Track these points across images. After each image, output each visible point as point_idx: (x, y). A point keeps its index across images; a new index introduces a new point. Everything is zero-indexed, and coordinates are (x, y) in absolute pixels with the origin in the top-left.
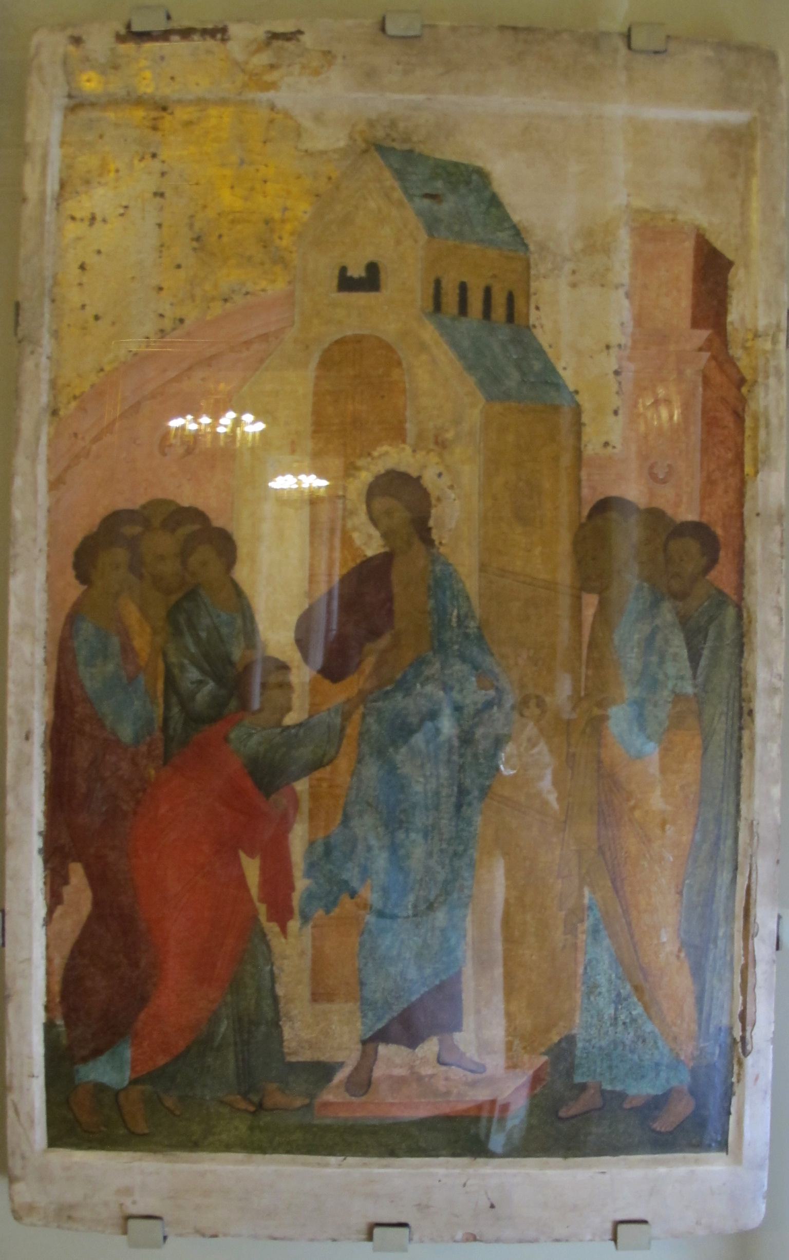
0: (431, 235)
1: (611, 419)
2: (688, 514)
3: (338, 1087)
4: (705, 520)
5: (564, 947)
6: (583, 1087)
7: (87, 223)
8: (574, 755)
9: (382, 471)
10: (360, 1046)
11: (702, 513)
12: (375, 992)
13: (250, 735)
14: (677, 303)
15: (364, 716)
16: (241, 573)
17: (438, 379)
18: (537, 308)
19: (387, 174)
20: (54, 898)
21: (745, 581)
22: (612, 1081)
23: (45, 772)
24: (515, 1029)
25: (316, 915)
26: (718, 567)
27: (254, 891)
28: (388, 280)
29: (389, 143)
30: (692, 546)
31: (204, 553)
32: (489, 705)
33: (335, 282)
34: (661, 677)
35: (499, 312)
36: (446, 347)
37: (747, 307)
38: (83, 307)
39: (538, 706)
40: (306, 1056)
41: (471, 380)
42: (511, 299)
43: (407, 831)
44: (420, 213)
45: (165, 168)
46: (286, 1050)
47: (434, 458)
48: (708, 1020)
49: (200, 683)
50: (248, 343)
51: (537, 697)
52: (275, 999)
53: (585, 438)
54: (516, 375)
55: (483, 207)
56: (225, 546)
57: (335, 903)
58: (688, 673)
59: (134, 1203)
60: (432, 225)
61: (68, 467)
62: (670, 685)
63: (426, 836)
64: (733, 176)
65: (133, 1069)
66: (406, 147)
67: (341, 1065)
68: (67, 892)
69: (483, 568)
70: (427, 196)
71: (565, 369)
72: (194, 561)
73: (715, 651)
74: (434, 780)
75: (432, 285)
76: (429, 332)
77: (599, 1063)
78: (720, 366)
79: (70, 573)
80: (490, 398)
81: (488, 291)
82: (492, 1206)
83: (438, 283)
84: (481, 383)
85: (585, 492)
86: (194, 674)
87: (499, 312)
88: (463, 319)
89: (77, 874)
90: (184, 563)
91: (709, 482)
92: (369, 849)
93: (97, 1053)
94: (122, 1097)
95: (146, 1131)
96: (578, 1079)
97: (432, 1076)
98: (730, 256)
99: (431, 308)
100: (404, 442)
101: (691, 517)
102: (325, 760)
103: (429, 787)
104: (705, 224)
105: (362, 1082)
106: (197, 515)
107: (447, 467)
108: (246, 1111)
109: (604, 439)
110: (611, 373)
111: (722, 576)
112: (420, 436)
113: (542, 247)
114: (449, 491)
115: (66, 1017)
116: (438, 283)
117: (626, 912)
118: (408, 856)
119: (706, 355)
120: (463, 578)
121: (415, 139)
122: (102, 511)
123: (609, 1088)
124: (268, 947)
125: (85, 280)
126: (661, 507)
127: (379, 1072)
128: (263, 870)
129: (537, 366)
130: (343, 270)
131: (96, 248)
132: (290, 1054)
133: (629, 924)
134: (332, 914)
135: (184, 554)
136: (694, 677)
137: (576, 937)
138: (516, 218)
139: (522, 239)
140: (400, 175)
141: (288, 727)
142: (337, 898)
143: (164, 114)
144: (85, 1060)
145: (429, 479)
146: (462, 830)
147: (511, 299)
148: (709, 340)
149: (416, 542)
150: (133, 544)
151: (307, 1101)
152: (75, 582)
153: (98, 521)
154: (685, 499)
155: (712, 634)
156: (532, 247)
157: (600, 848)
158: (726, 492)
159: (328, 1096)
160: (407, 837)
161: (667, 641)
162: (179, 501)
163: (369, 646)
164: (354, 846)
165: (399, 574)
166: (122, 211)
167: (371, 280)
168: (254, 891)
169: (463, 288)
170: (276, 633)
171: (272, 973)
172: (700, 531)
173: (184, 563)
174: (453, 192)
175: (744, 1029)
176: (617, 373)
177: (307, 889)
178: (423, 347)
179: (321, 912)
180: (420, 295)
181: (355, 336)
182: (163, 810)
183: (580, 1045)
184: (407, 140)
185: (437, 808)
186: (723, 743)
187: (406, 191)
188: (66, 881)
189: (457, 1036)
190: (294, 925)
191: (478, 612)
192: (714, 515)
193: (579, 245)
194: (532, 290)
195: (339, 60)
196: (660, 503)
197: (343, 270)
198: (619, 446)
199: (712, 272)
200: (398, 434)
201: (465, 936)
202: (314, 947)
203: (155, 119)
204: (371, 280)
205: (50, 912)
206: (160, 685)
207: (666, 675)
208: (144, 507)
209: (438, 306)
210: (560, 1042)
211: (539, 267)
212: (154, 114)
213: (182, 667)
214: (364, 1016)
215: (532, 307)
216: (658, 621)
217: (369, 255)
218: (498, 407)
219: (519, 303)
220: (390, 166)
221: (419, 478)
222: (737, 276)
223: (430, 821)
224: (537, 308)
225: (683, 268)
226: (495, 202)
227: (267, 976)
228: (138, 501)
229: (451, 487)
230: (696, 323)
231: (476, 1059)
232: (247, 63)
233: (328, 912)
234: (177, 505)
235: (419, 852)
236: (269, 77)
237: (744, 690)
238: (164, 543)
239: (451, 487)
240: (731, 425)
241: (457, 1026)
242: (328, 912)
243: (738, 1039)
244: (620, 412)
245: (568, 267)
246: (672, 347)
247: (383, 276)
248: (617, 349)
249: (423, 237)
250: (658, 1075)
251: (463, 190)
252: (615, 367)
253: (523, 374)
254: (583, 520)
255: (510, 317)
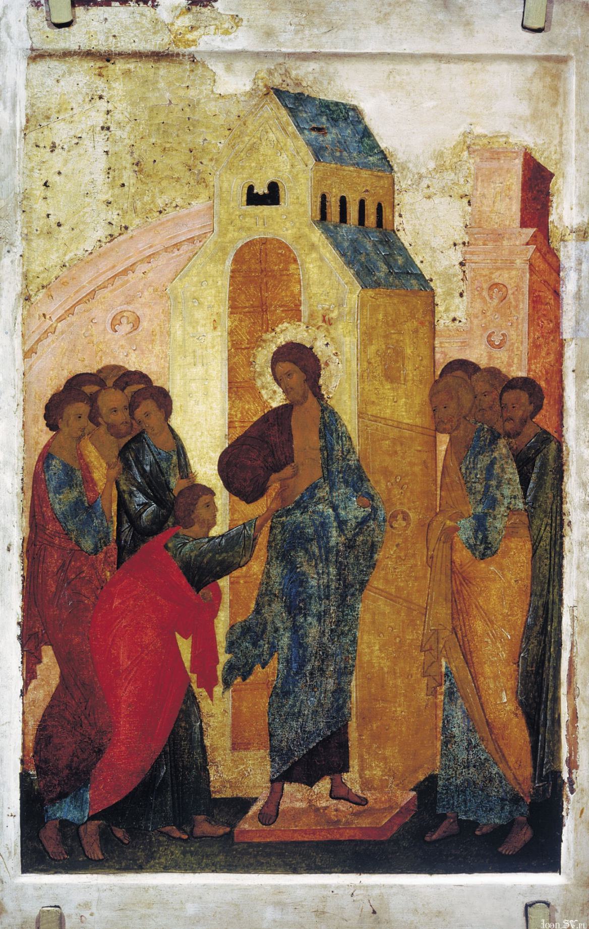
0: (318, 160)
1: (458, 300)
2: (518, 371)
3: (252, 817)
4: (531, 376)
5: (427, 705)
6: (444, 817)
7: (48, 149)
8: (432, 557)
9: (283, 343)
10: (269, 785)
11: (529, 370)
12: (281, 741)
13: (185, 544)
14: (508, 206)
15: (272, 528)
16: (176, 421)
17: (324, 276)
18: (400, 216)
19: (284, 112)
20: (29, 674)
21: (564, 422)
22: (466, 813)
23: (23, 576)
24: (390, 770)
25: (235, 682)
26: (543, 412)
27: (187, 664)
28: (286, 195)
29: (284, 88)
30: (524, 397)
31: (148, 406)
32: (365, 521)
33: (245, 198)
34: (499, 496)
35: (371, 220)
36: (330, 247)
37: (565, 212)
38: (48, 215)
39: (404, 519)
40: (228, 794)
41: (350, 273)
42: (380, 209)
43: (305, 616)
44: (309, 143)
45: (110, 107)
46: (212, 789)
47: (321, 334)
48: (542, 766)
49: (145, 505)
50: (177, 246)
51: (403, 512)
52: (204, 748)
53: (437, 316)
54: (384, 268)
55: (358, 137)
56: (162, 400)
57: (250, 673)
58: (520, 493)
59: (92, 915)
60: (318, 153)
61: (39, 340)
62: (506, 502)
63: (319, 620)
64: (554, 104)
65: (91, 807)
66: (298, 90)
67: (255, 800)
68: (40, 668)
69: (361, 415)
70: (313, 129)
71: (422, 262)
72: (139, 413)
73: (541, 477)
74: (325, 576)
75: (319, 199)
76: (317, 236)
77: (456, 797)
78: (544, 257)
79: (42, 422)
80: (364, 286)
81: (362, 203)
82: (374, 912)
83: (324, 197)
84: (357, 274)
85: (438, 356)
86: (141, 498)
87: (371, 220)
88: (344, 225)
89: (48, 655)
90: (132, 414)
91: (535, 347)
92: (276, 630)
93: (62, 796)
94: (82, 829)
95: (101, 857)
96: (440, 811)
97: (326, 808)
98: (551, 169)
99: (318, 218)
100: (300, 320)
101: (523, 374)
102: (242, 563)
103: (321, 582)
104: (532, 146)
105: (269, 815)
106: (142, 377)
107: (332, 339)
108: (180, 839)
109: (452, 315)
110: (457, 263)
111: (545, 419)
112: (312, 316)
113: (404, 168)
114: (335, 357)
115: (37, 768)
116: (324, 197)
117: (475, 679)
118: (306, 635)
119: (532, 248)
120: (346, 423)
121: (304, 84)
122: (65, 375)
123: (464, 818)
124: (198, 708)
125: (49, 194)
126: (498, 367)
127: (285, 804)
128: (194, 647)
129: (400, 261)
130: (251, 188)
131: (57, 170)
132: (215, 792)
133: (477, 688)
134: (248, 681)
135: (132, 407)
136: (525, 497)
137: (436, 697)
138: (383, 146)
139: (388, 162)
140: (293, 112)
141: (214, 538)
142: (252, 669)
143: (108, 64)
144: (52, 802)
145: (319, 348)
146: (347, 615)
147: (380, 209)
148: (534, 236)
149: (310, 396)
150: (92, 400)
151: (228, 829)
152: (46, 429)
153: (64, 382)
154: (516, 360)
155: (538, 463)
156: (396, 169)
157: (454, 628)
158: (548, 354)
159: (245, 825)
160: (305, 620)
161: (503, 470)
162: (127, 366)
163: (274, 476)
164: (265, 629)
165: (296, 421)
166: (76, 141)
167: (272, 196)
168: (187, 664)
169: (343, 201)
170: (205, 469)
171: (201, 727)
172: (527, 384)
173: (132, 414)
174: (334, 128)
175: (570, 773)
176: (462, 264)
177: (229, 662)
178: (313, 247)
179: (239, 680)
180: (308, 207)
181: (261, 239)
182: (116, 602)
183: (440, 783)
184: (298, 84)
185: (327, 597)
186: (548, 547)
187: (298, 126)
188: (40, 661)
189: (345, 776)
190: (218, 690)
191: (357, 449)
192: (537, 371)
193: (432, 165)
194: (396, 202)
195: (245, 23)
196: (496, 364)
197: (251, 188)
198: (464, 321)
199: (537, 183)
200: (294, 313)
201: (350, 697)
202: (233, 707)
203: (100, 68)
204: (272, 196)
205: (26, 684)
206: (115, 507)
207: (503, 495)
208: (99, 371)
209: (324, 216)
210: (424, 780)
211: (402, 182)
212: (100, 64)
213: (131, 493)
214: (273, 760)
215: (397, 214)
216: (496, 454)
217: (271, 178)
218: (371, 293)
219: (386, 212)
220: (286, 106)
221: (311, 348)
222: (556, 185)
223: (323, 608)
224: (400, 216)
225: (513, 178)
226: (367, 133)
227: (197, 730)
228: (92, 367)
229: (336, 354)
230: (524, 224)
231: (360, 793)
232: (172, 24)
233: (244, 679)
234: (126, 369)
235: (314, 632)
236: (190, 37)
237: (564, 506)
238: (112, 400)
239: (336, 354)
240: (552, 302)
241: (346, 768)
242: (244, 679)
243: (566, 780)
244: (465, 294)
245: (425, 182)
246: (505, 243)
247: (281, 193)
248: (462, 246)
249: (312, 161)
250: (502, 808)
251: (342, 124)
252: (461, 259)
253: (390, 266)
254: (437, 378)
255: (379, 224)
